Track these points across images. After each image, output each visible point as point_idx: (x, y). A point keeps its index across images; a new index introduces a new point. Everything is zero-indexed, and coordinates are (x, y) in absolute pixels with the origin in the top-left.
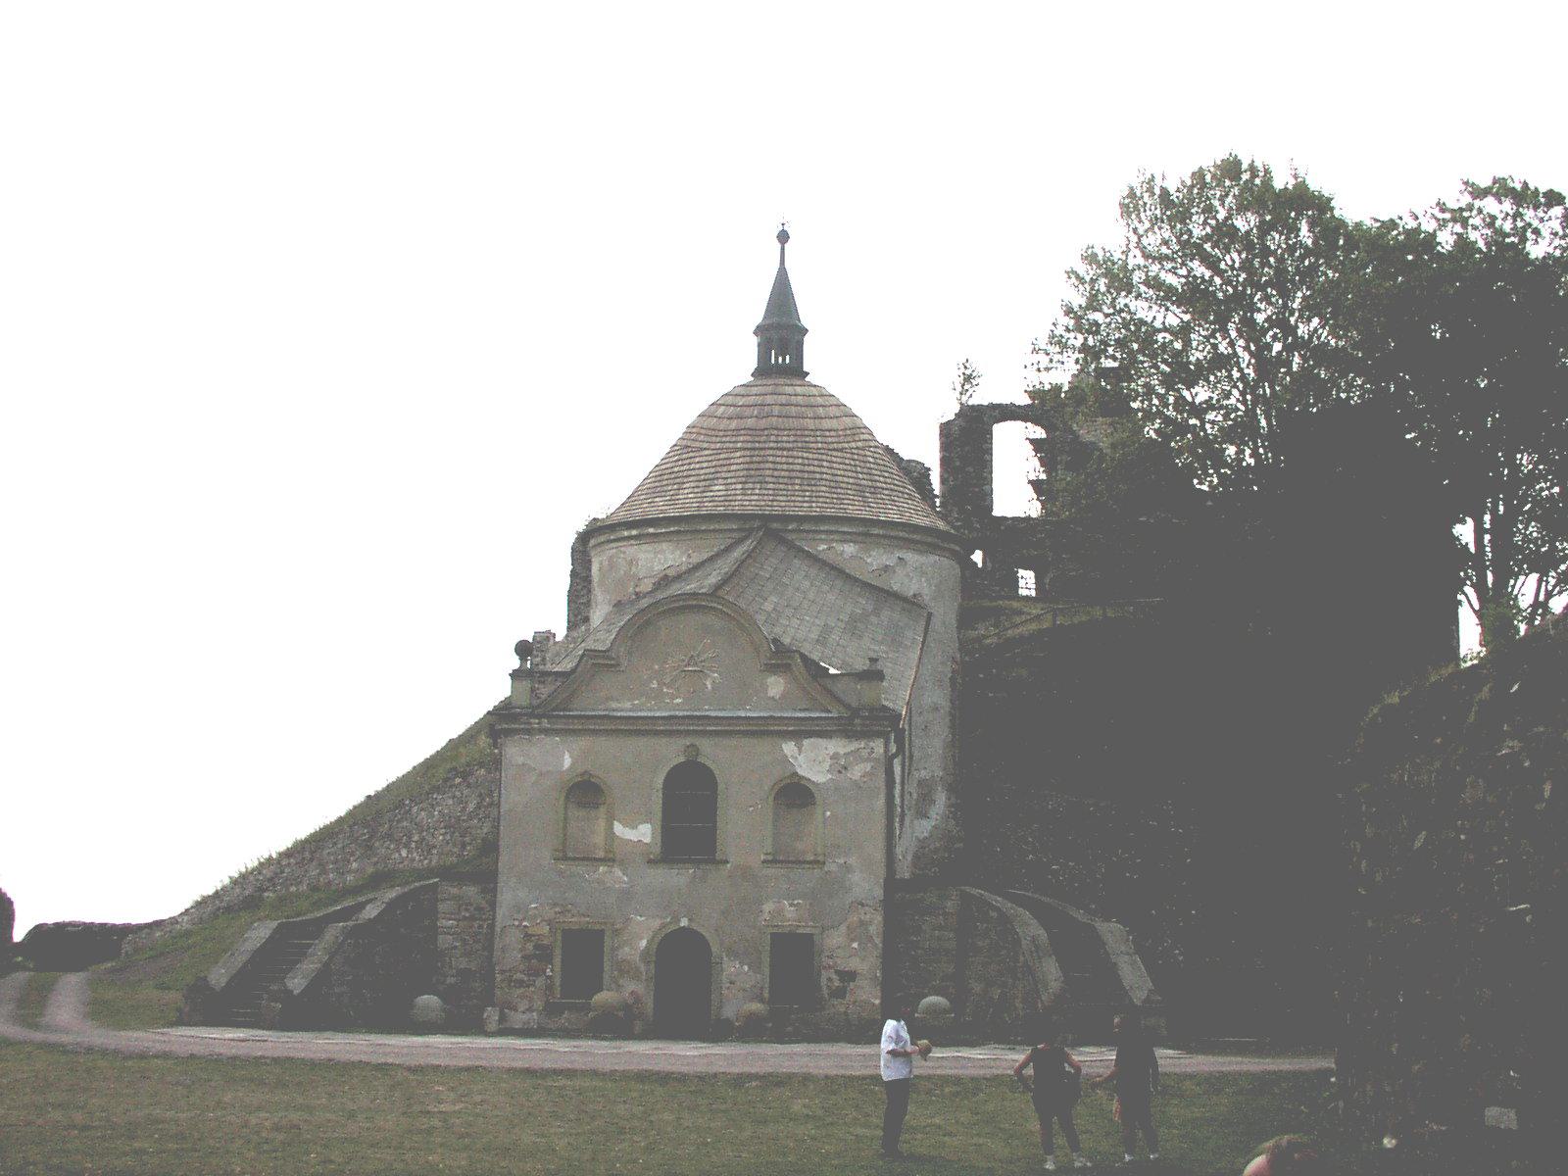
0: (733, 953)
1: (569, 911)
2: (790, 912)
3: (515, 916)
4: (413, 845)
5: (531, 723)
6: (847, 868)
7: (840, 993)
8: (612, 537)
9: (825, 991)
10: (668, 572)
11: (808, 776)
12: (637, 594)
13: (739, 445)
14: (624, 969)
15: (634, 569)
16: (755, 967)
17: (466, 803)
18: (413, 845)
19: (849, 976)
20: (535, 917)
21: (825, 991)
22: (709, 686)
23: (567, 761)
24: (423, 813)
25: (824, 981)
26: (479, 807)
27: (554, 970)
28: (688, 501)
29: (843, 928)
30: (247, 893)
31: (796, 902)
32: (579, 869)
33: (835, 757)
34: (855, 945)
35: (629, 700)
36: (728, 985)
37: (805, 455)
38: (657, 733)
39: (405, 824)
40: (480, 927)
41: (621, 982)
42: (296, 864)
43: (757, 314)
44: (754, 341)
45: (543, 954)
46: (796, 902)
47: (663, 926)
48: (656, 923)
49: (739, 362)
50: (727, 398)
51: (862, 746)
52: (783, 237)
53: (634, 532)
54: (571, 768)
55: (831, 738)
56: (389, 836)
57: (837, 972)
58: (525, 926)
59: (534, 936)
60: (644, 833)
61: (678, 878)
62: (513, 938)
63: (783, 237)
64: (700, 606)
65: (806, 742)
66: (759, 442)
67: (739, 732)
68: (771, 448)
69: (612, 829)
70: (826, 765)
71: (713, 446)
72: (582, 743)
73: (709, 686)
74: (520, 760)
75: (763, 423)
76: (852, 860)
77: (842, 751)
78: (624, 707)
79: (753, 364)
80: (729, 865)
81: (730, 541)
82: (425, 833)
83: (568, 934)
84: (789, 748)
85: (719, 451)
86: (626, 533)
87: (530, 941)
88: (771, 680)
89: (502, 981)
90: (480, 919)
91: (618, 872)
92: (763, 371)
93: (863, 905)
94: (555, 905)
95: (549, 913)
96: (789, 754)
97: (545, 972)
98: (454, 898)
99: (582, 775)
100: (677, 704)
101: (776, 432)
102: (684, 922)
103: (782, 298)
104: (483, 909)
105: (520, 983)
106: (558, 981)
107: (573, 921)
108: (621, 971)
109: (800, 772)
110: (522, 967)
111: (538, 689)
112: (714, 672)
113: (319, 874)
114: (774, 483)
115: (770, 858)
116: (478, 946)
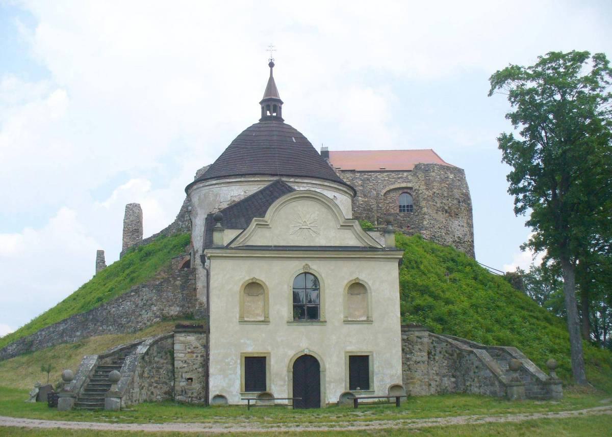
40: (197, 356)
43: (261, 96)
44: (260, 107)
52: (271, 65)
63: (271, 65)
79: (260, 117)
92: (264, 118)
98: (183, 343)
99: (252, 279)
103: (271, 86)
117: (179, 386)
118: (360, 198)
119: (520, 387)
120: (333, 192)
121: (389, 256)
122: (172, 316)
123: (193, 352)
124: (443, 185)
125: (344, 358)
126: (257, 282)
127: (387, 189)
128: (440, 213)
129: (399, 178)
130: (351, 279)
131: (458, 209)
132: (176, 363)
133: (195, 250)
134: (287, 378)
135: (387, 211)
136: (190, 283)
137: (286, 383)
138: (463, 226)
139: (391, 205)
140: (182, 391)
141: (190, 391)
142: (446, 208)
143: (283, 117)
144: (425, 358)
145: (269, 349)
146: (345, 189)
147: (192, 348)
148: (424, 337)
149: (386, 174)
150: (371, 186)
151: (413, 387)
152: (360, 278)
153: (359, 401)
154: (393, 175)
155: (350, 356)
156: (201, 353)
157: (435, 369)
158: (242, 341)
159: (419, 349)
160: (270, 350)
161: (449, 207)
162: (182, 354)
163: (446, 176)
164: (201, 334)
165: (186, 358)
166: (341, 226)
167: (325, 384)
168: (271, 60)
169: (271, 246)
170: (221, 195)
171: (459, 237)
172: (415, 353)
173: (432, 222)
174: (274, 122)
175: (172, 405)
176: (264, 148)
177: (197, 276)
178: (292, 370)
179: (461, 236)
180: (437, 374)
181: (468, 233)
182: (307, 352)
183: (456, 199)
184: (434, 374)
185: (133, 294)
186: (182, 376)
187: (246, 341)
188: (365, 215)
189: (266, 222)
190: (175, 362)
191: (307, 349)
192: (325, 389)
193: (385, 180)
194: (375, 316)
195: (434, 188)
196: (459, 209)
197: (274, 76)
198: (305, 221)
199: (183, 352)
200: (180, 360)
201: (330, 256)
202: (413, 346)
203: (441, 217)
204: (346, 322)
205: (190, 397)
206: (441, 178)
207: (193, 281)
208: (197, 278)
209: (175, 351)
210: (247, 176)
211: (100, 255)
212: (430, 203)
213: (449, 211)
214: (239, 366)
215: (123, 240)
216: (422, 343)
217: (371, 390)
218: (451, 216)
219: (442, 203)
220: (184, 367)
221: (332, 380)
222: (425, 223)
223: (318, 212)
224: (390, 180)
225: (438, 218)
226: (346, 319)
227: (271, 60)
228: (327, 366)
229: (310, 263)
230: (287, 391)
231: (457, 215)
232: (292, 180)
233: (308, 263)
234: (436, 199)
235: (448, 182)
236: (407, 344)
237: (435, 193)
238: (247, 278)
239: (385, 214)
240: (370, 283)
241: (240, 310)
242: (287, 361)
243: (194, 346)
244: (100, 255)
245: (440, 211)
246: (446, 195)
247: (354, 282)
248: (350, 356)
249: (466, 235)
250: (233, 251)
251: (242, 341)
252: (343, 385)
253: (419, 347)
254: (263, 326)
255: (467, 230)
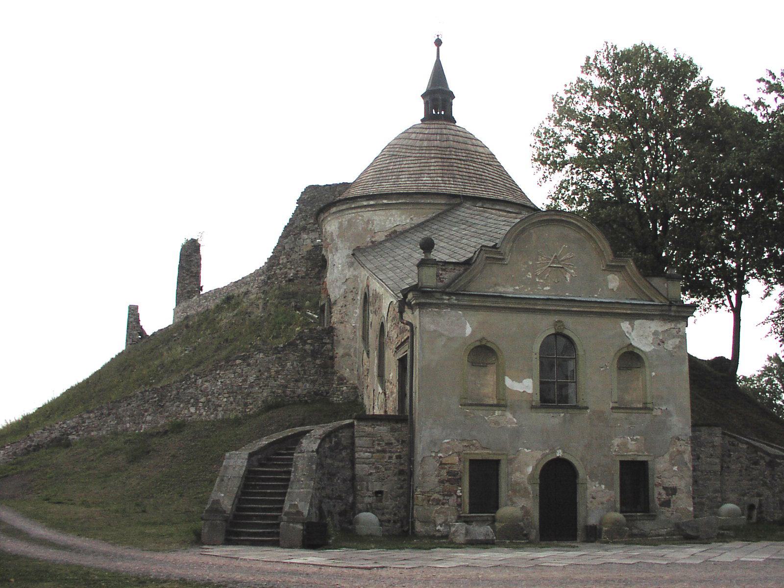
0: (593, 476)
1: (473, 445)
2: (632, 445)
3: (433, 449)
4: (200, 405)
5: (443, 299)
6: (668, 413)
7: (667, 504)
8: (353, 206)
9: (657, 502)
10: (396, 228)
11: (640, 346)
12: (372, 242)
13: (432, 155)
14: (517, 490)
15: (370, 226)
16: (609, 486)
17: (247, 376)
18: (200, 405)
19: (673, 491)
20: (448, 449)
21: (657, 502)
22: (568, 279)
23: (468, 330)
24: (207, 384)
25: (656, 495)
26: (258, 378)
27: (464, 491)
28: (406, 184)
29: (667, 457)
30: (53, 436)
31: (635, 438)
32: (480, 412)
33: (656, 333)
34: (675, 468)
35: (512, 286)
36: (591, 499)
37: (474, 165)
38: (534, 311)
39: (190, 391)
40: (390, 458)
41: (515, 500)
42: (96, 417)
43: (423, 85)
45: (454, 478)
46: (635, 438)
47: (544, 456)
48: (538, 454)
49: (416, 112)
50: (403, 135)
51: (673, 326)
52: (438, 43)
53: (372, 202)
54: (471, 335)
55: (653, 320)
56: (178, 398)
57: (664, 488)
58: (441, 457)
59: (446, 464)
60: (527, 386)
61: (552, 419)
62: (431, 466)
63: (438, 43)
64: (562, 221)
65: (637, 322)
66: (446, 155)
67: (592, 313)
68: (454, 159)
69: (504, 382)
70: (650, 339)
71: (414, 155)
72: (481, 316)
73: (568, 279)
74: (432, 327)
75: (444, 144)
76: (671, 408)
77: (660, 329)
78: (509, 290)
80: (588, 411)
81: (440, 211)
82: (210, 397)
83: (473, 462)
84: (625, 326)
85: (420, 158)
86: (365, 203)
87: (443, 468)
88: (610, 277)
89: (423, 500)
90: (390, 452)
91: (509, 415)
92: (429, 117)
93: (679, 440)
94: (463, 440)
95: (459, 447)
96: (625, 330)
97: (455, 493)
98: (368, 435)
99: (481, 340)
100: (546, 290)
101: (454, 150)
102: (559, 453)
103: (438, 74)
104: (391, 444)
105: (438, 502)
106: (467, 500)
107: (480, 454)
108: (515, 491)
109: (633, 344)
110: (438, 489)
111: (441, 274)
112: (571, 269)
113: (117, 424)
114: (461, 179)
115: (616, 405)
116: (389, 472)
117: (363, 502)
122: (298, 396)
123: (384, 451)
126: (489, 345)
132: (358, 467)
133: (332, 300)
136: (324, 348)
143: (455, 114)
156: (397, 452)
164: (397, 422)
166: (607, 265)
168: (438, 36)
170: (375, 222)
177: (335, 338)
178: (538, 481)
185: (238, 362)
190: (357, 466)
197: (441, 58)
207: (329, 346)
208: (335, 342)
209: (356, 449)
210: (415, 196)
211: (133, 313)
215: (224, 287)
227: (438, 36)
244: (133, 313)
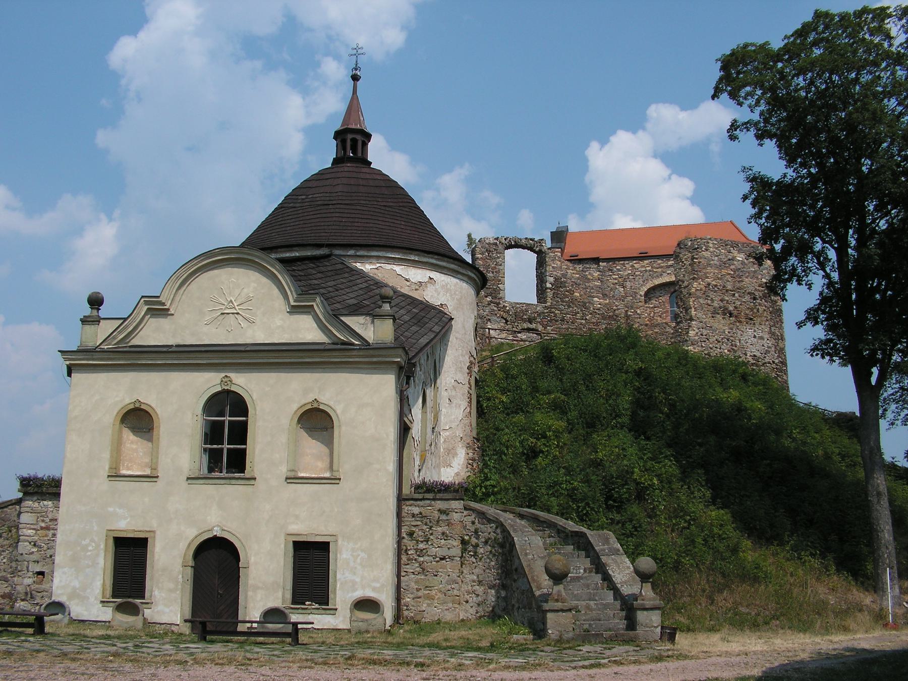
63: (355, 78)
99: (134, 403)
118: (596, 299)
119: (560, 613)
120: (428, 271)
121: (375, 360)
124: (724, 272)
125: (283, 546)
126: (143, 407)
127: (650, 285)
128: (719, 317)
129: (668, 267)
130: (304, 402)
131: (752, 310)
134: (180, 576)
135: (650, 320)
137: (180, 587)
138: (762, 338)
139: (657, 310)
140: (26, 593)
141: (39, 594)
142: (731, 308)
144: (456, 551)
145: (154, 525)
146: (452, 266)
147: (47, 520)
148: (453, 510)
149: (646, 262)
150: (616, 279)
151: (429, 605)
152: (322, 399)
153: (300, 626)
154: (660, 262)
155: (293, 541)
157: (476, 571)
158: (111, 509)
159: (443, 534)
160: (155, 525)
161: (736, 307)
162: (32, 531)
163: (730, 257)
165: (36, 538)
167: (246, 592)
169: (172, 346)
171: (755, 356)
172: (435, 540)
173: (705, 332)
174: (349, 165)
175: (789, 651)
176: (319, 205)
179: (758, 354)
180: (480, 583)
181: (773, 349)
182: (217, 532)
183: (749, 293)
184: (474, 581)
186: (28, 568)
187: (117, 510)
188: (604, 327)
189: (164, 304)
191: (218, 526)
192: (246, 597)
193: (646, 271)
194: (345, 468)
195: (707, 277)
196: (755, 310)
198: (231, 301)
199: (32, 527)
200: (28, 541)
201: (292, 360)
202: (431, 528)
203: (721, 324)
204: (293, 479)
205: (37, 604)
206: (720, 260)
210: (279, 250)
212: (701, 301)
213: (735, 313)
214: (102, 554)
216: (449, 524)
217: (330, 606)
218: (740, 322)
219: (722, 300)
220: (33, 553)
221: (260, 585)
222: (691, 333)
223: (256, 285)
224: (654, 270)
225: (716, 325)
226: (292, 474)
228: (252, 560)
229: (232, 375)
230: (179, 601)
231: (751, 319)
232: (351, 252)
233: (228, 375)
234: (712, 295)
235: (732, 267)
236: (419, 523)
237: (709, 284)
238: (127, 401)
239: (646, 325)
240: (339, 409)
241: (112, 456)
242: (183, 546)
243: (50, 517)
245: (718, 314)
246: (729, 287)
247: (309, 407)
248: (293, 541)
249: (767, 352)
250: (105, 355)
251: (111, 509)
252: (280, 594)
253: (445, 529)
254: (146, 485)
255: (770, 345)
